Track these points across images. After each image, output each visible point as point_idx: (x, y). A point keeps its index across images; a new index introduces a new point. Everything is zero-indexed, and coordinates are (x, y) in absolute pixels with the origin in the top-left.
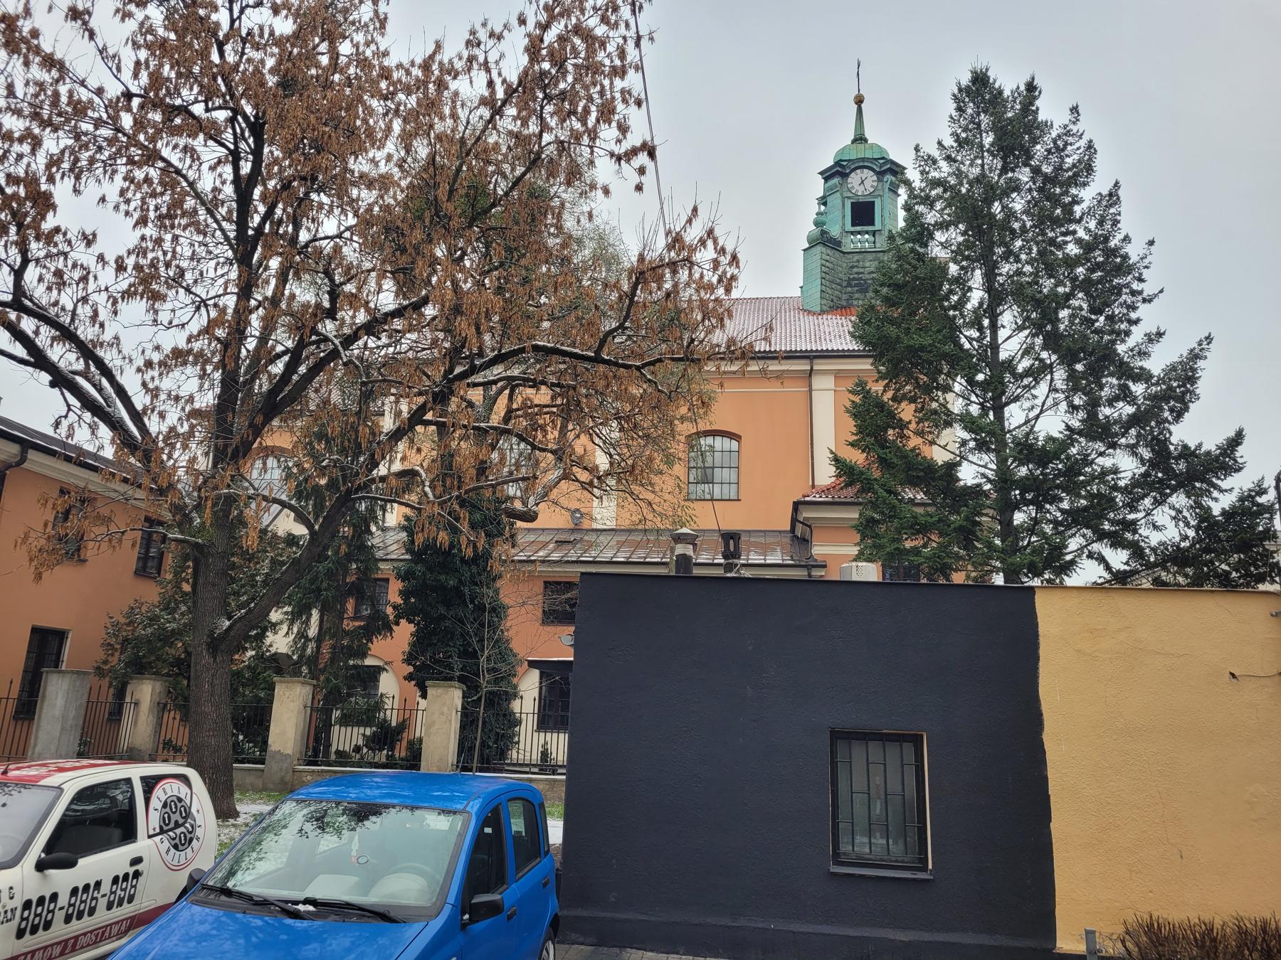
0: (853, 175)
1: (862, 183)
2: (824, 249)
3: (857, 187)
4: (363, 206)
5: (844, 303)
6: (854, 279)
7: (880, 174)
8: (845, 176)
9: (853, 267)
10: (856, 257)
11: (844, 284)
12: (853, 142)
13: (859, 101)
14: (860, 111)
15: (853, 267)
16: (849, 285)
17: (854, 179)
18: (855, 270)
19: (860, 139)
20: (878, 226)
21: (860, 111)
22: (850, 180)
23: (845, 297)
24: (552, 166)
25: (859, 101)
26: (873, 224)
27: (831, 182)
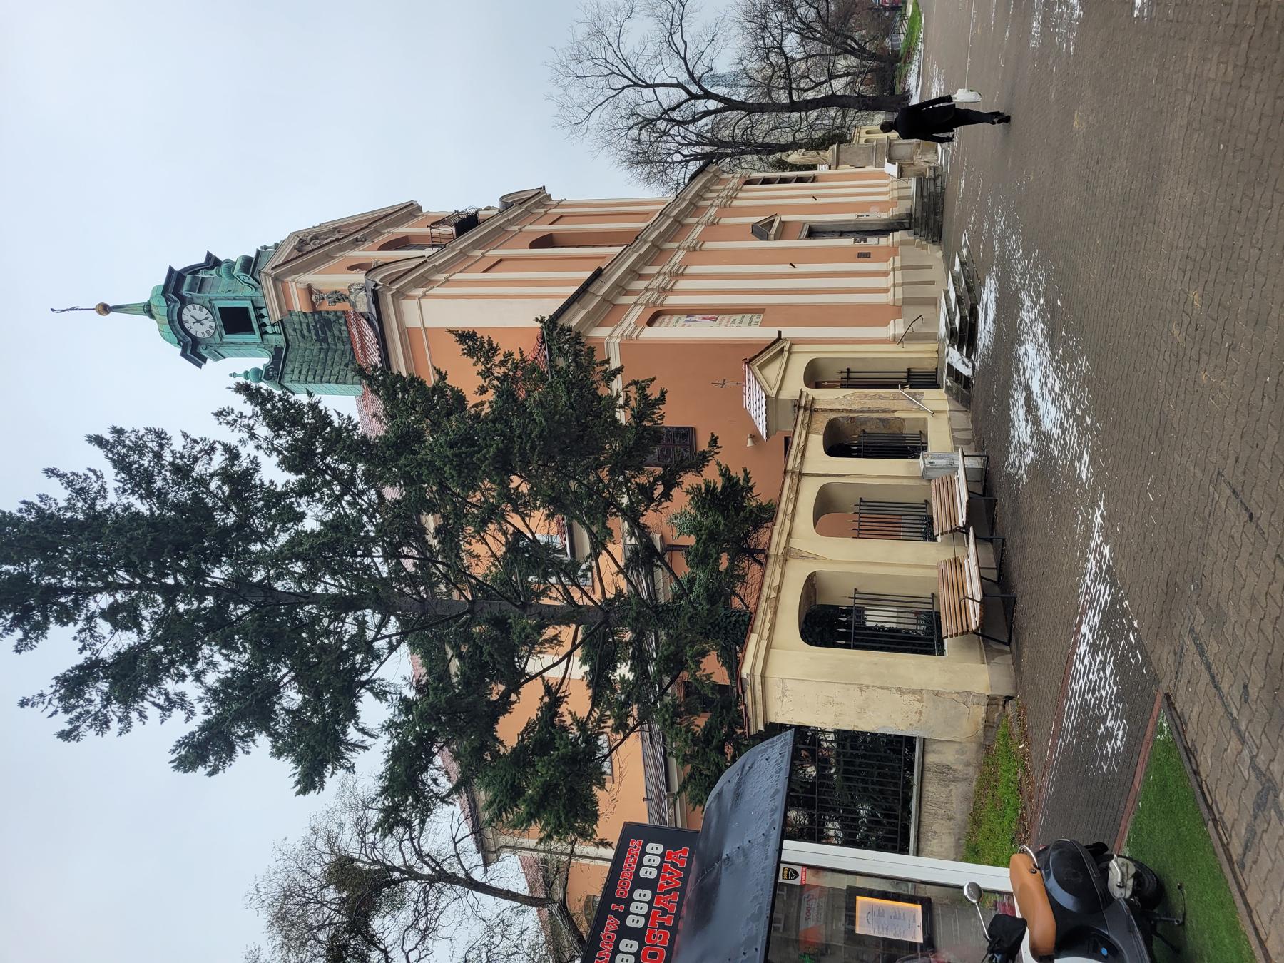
0: (193, 332)
1: (201, 322)
2: (287, 378)
3: (206, 328)
4: (302, 504)
5: (348, 346)
6: (317, 334)
7: (184, 301)
8: (196, 341)
9: (303, 336)
10: (290, 331)
11: (325, 346)
12: (152, 317)
13: (105, 309)
14: (118, 309)
15: (303, 336)
16: (325, 340)
17: (198, 331)
18: (306, 333)
19: (148, 310)
20: (248, 304)
21: (118, 309)
22: (200, 335)
23: (340, 346)
24: (252, 475)
25: (105, 309)
26: (246, 309)
27: (204, 353)
